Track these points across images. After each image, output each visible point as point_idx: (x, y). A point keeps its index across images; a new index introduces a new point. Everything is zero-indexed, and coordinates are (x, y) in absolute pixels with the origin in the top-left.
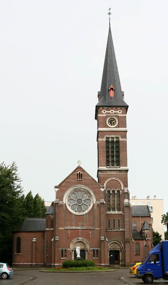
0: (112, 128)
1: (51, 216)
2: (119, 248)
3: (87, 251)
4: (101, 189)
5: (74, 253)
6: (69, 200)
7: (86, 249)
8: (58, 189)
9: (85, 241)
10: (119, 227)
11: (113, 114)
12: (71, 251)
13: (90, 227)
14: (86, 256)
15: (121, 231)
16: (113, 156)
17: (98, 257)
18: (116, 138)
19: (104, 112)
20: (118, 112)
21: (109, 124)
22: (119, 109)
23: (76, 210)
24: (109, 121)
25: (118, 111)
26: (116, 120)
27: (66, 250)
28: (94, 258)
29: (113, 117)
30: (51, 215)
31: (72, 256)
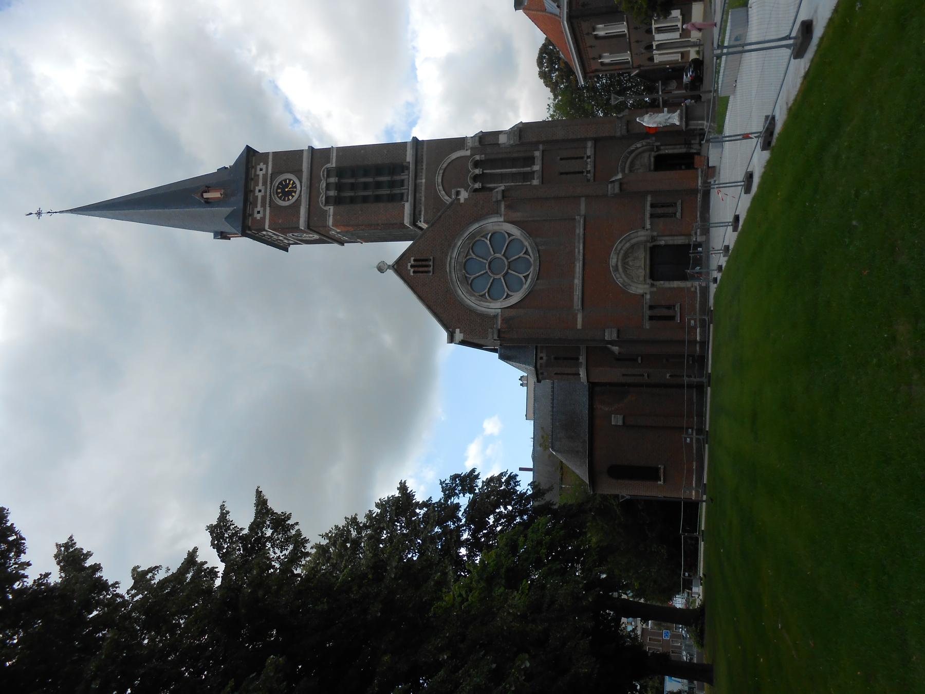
0: (301, 188)
1: (541, 361)
2: (646, 155)
3: (653, 239)
4: (462, 201)
5: (662, 282)
6: (491, 298)
7: (647, 241)
8: (458, 330)
9: (622, 245)
10: (582, 158)
11: (266, 189)
12: (655, 289)
13: (577, 231)
14: (670, 240)
15: (593, 152)
16: (379, 185)
17: (675, 204)
18: (328, 176)
19: (259, 212)
20: (261, 174)
21: (290, 197)
22: (256, 171)
23: (521, 276)
24: (284, 200)
25: (258, 175)
26: (280, 181)
27: (651, 307)
28: (678, 215)
29: (275, 188)
30: (539, 362)
31: (672, 286)
